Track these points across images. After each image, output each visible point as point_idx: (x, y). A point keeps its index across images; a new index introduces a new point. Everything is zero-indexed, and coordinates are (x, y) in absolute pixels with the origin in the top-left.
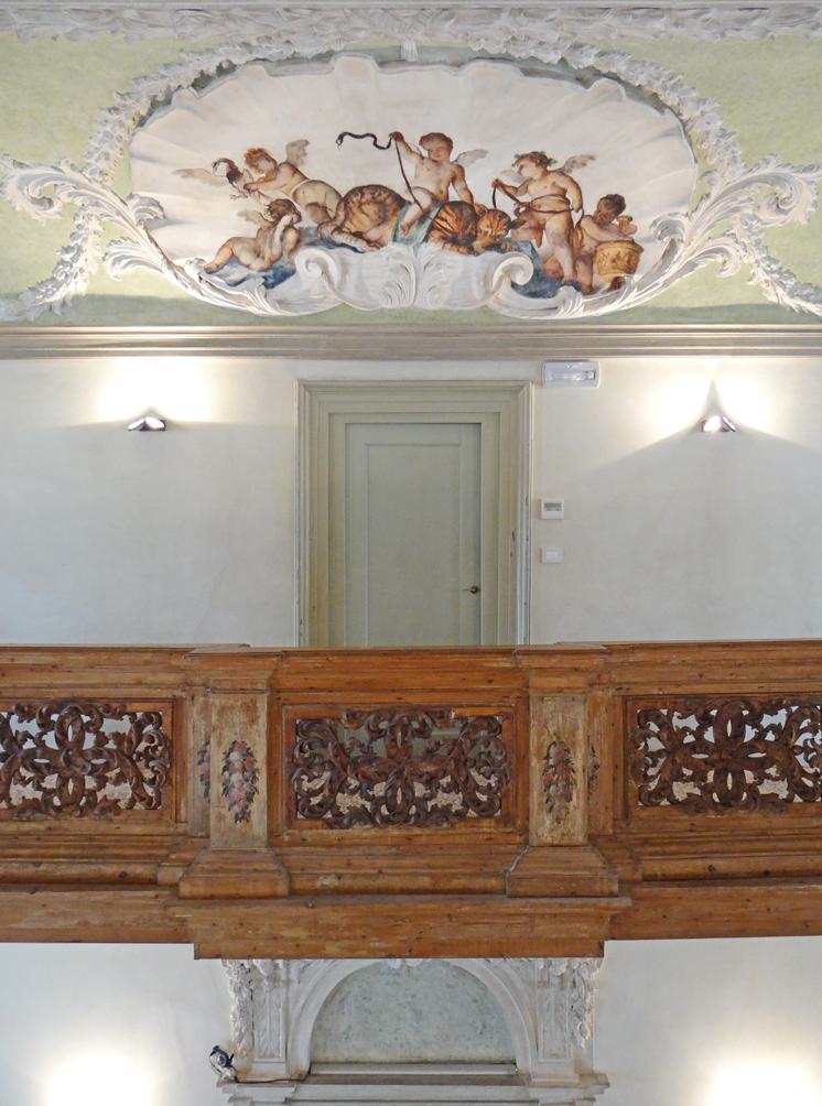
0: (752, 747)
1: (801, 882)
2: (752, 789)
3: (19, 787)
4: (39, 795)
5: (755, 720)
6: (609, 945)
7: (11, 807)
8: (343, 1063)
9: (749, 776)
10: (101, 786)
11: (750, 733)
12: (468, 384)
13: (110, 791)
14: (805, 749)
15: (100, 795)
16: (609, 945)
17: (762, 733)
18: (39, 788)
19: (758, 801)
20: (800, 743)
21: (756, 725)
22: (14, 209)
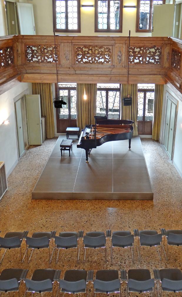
0: (140, 57)
1: (116, 15)
2: (141, 50)
3: (84, 59)
4: (37, 60)
5: (140, 61)
6: (97, 147)
7: (83, 62)
8: (95, 91)
9: (141, 52)
10: (99, 59)
11: (141, 59)
12: (21, 131)
13: (100, 60)
14: (132, 56)
15: (98, 61)
16: (97, 147)
17: (139, 59)
18: (88, 59)
19: (140, 48)
20: (133, 57)
21: (140, 60)
22: (109, 207)
